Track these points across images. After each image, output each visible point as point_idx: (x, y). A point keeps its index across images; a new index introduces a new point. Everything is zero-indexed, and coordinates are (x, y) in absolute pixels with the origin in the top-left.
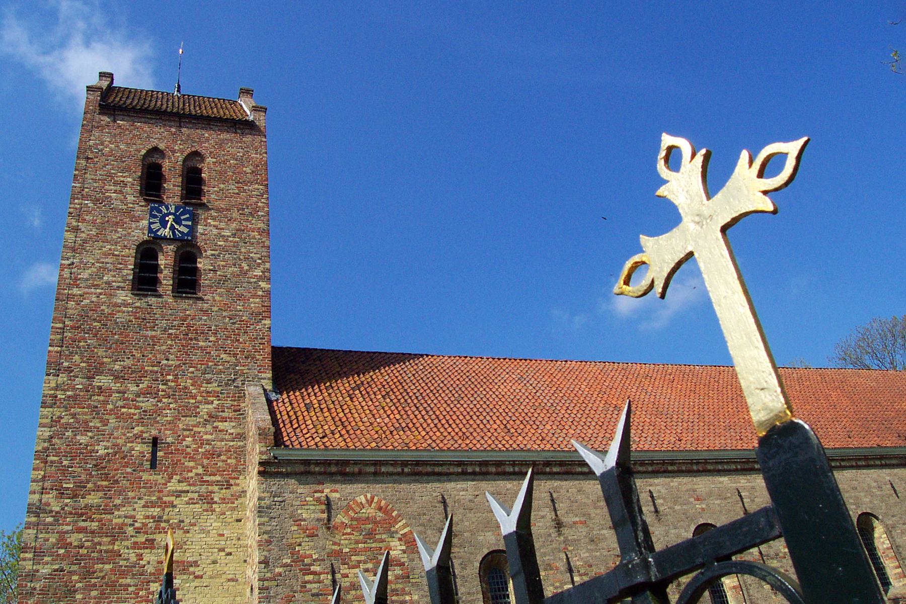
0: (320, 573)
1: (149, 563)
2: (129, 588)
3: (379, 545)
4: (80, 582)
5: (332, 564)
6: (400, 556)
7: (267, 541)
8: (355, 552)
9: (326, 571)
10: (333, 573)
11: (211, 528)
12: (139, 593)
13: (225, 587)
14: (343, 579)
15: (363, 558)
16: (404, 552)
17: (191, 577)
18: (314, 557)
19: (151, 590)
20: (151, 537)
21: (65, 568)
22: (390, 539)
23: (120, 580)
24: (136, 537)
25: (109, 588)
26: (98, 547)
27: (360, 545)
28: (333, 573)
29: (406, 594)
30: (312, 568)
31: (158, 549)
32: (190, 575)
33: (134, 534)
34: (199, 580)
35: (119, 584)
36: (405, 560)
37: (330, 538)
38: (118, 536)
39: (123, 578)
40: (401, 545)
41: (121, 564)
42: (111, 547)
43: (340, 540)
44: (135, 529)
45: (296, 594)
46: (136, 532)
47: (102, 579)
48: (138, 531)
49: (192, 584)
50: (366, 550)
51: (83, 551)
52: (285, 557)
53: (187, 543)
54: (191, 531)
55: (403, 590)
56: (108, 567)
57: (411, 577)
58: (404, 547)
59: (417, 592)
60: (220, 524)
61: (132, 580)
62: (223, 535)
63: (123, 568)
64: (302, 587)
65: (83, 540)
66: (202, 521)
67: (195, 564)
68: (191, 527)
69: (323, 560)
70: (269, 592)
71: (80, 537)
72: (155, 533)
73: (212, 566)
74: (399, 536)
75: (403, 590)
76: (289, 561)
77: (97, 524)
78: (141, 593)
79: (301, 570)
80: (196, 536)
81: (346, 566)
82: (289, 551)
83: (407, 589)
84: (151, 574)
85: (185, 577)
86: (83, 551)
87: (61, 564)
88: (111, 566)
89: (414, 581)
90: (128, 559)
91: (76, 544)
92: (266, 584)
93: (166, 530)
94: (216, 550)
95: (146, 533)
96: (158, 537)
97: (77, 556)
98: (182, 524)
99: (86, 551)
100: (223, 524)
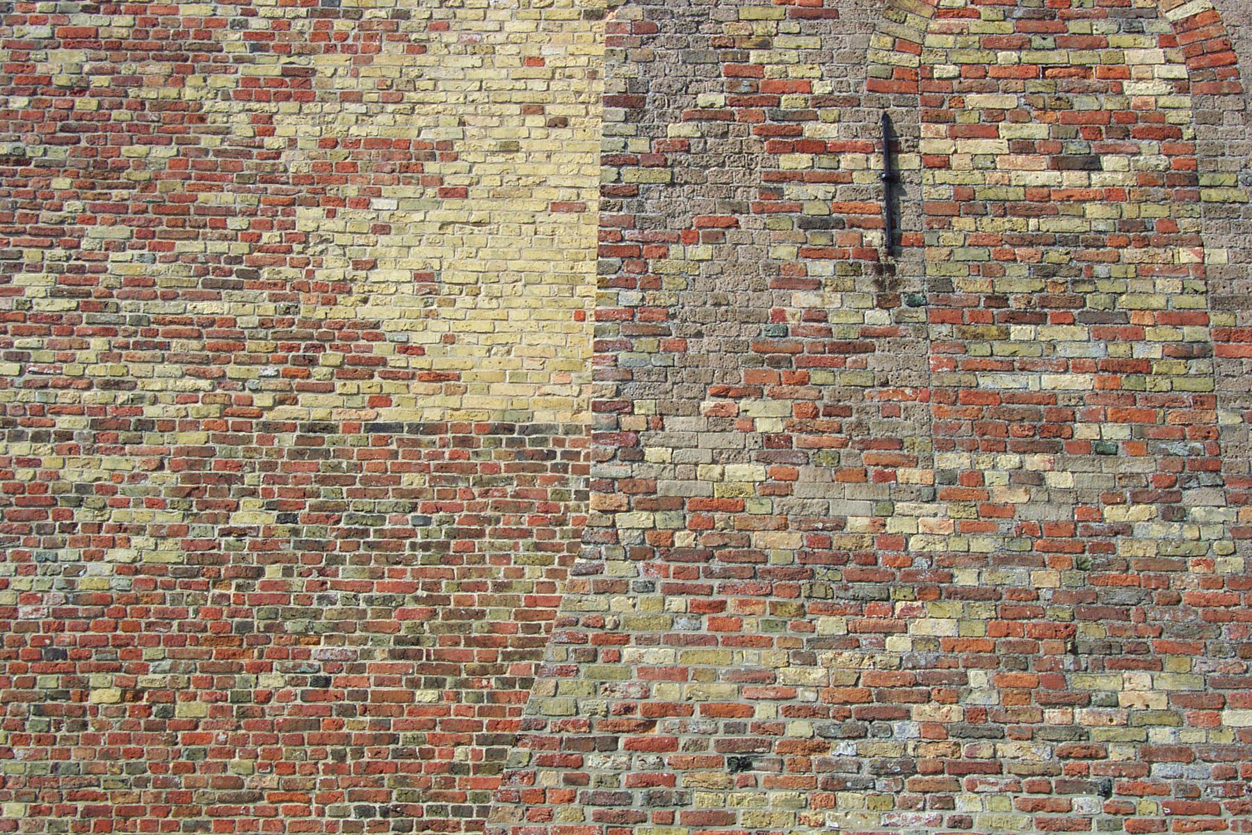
0: (838, 150)
1: (292, 143)
2: (229, 220)
3: (1076, 58)
4: (78, 198)
5: (886, 118)
6: (1161, 101)
7: (638, 28)
8: (982, 78)
9: (861, 141)
10: (891, 148)
11: (500, 37)
12: (260, 236)
13: (541, 229)
14: (928, 174)
15: (1010, 102)
16: (1181, 86)
17: (431, 192)
18: (819, 89)
19: (300, 227)
20: (301, 62)
21: (29, 154)
22: (1127, 39)
23: (202, 196)
24: (252, 61)
25: (165, 218)
26: (132, 92)
27: (1001, 55)
28: (891, 148)
29: (1181, 242)
30: (810, 129)
31: (323, 100)
32: (426, 185)
33: (246, 53)
34: (456, 203)
35: (197, 208)
36: (1183, 116)
37: (883, 24)
38: (195, 60)
39: (210, 189)
40: (1169, 61)
41: (202, 145)
42: (172, 92)
43: (925, 33)
44: (248, 36)
45: (742, 219)
46: (254, 48)
47: (143, 190)
48: (259, 43)
49: (434, 215)
50: (1023, 72)
51: (85, 104)
52: (708, 85)
53: (421, 84)
54: (432, 47)
55: (1169, 225)
56: (162, 153)
57: (1203, 181)
58: (1181, 71)
59: (1224, 239)
60: (530, 26)
61: (239, 197)
62: (540, 61)
63: (211, 157)
64: (764, 192)
65: (87, 68)
66: (471, 14)
67: (445, 150)
68: (433, 35)
69: (854, 102)
70: (641, 205)
71: (76, 60)
72: (313, 52)
73: (500, 158)
74: (1166, 28)
75: (1169, 225)
76: (720, 100)
77: (128, 19)
78: (266, 236)
79: (764, 134)
80: (451, 61)
81: (943, 128)
82: (722, 67)
83: (1184, 223)
84: (299, 179)
85: (410, 191)
86: (85, 104)
87: (18, 139)
88: (171, 151)
89: (1215, 194)
90: (227, 131)
91: (62, 80)
92: (629, 174)
93: (350, 42)
94: (516, 109)
95: (286, 50)
96: (324, 64)
97: (67, 118)
98: (403, 24)
99: (93, 103)
100: (542, 25)
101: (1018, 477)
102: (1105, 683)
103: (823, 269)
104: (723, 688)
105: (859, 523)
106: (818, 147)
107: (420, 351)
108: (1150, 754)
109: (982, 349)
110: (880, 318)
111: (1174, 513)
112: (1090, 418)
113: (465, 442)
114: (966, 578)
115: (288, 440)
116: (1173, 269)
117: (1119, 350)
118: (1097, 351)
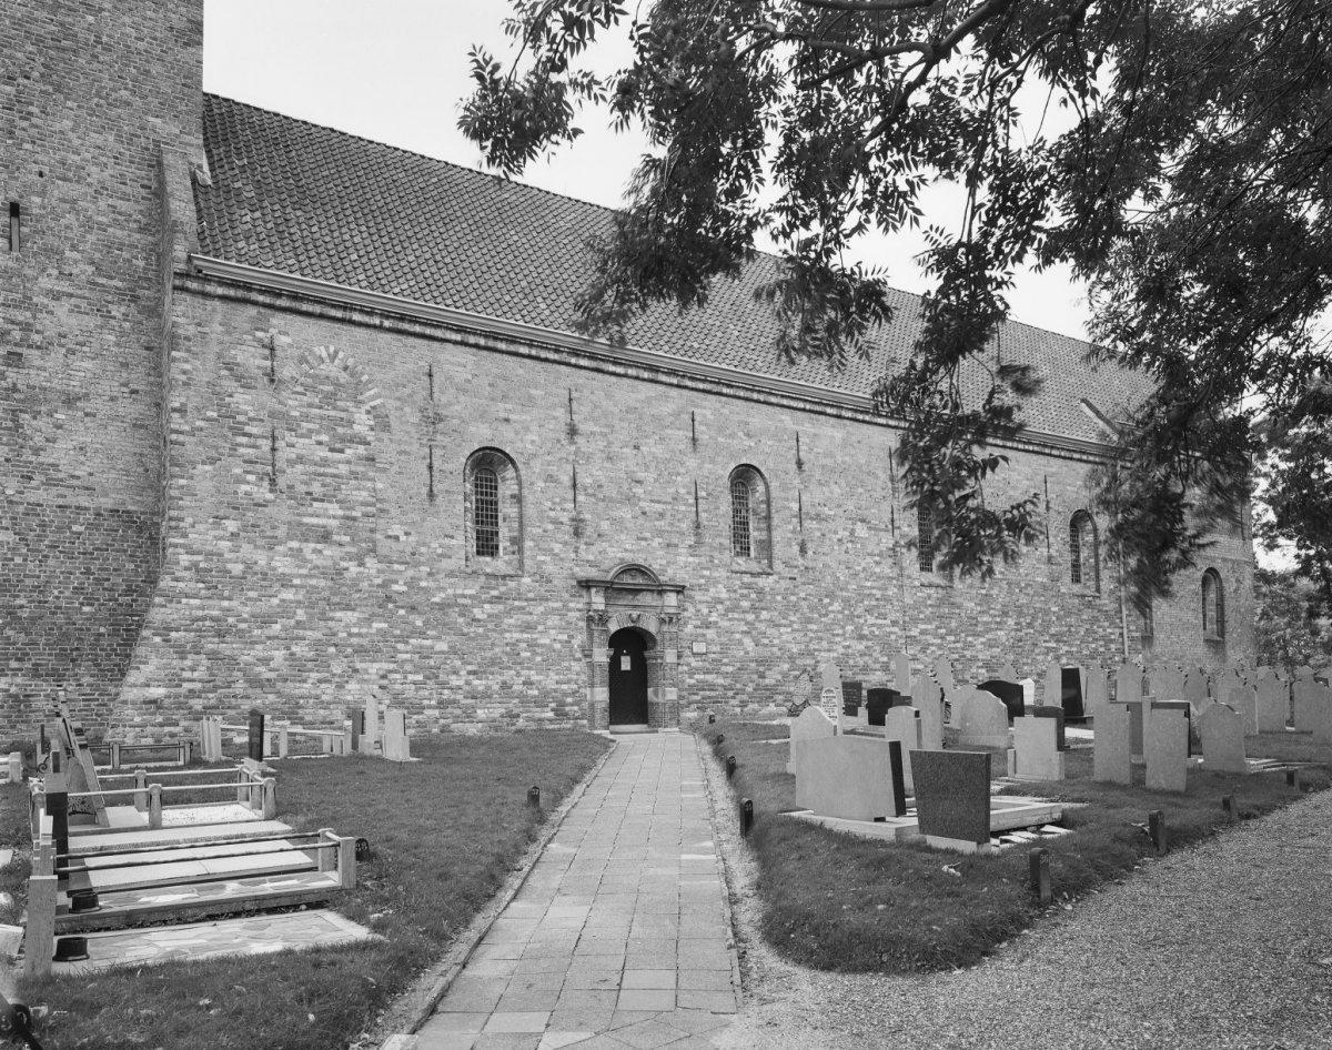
0: (257, 437)
8: (307, 418)
18: (251, 414)
30: (247, 429)
58: (372, 423)
101: (314, 551)
102: (339, 614)
103: (251, 478)
104: (215, 613)
105: (262, 562)
106: (249, 435)
107: (78, 478)
108: (350, 635)
109: (304, 509)
110: (270, 496)
111: (361, 564)
112: (338, 534)
113: (99, 514)
114: (297, 581)
115: (21, 509)
116: (365, 489)
117: (348, 513)
118: (341, 513)
